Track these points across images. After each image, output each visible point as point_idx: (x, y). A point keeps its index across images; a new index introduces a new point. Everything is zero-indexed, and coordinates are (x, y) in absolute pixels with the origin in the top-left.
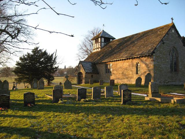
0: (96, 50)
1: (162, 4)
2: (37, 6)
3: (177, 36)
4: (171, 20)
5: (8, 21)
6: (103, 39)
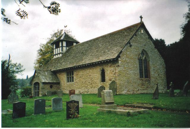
0: (59, 55)
2: (24, 6)
3: (147, 36)
4: (140, 18)
6: (65, 44)
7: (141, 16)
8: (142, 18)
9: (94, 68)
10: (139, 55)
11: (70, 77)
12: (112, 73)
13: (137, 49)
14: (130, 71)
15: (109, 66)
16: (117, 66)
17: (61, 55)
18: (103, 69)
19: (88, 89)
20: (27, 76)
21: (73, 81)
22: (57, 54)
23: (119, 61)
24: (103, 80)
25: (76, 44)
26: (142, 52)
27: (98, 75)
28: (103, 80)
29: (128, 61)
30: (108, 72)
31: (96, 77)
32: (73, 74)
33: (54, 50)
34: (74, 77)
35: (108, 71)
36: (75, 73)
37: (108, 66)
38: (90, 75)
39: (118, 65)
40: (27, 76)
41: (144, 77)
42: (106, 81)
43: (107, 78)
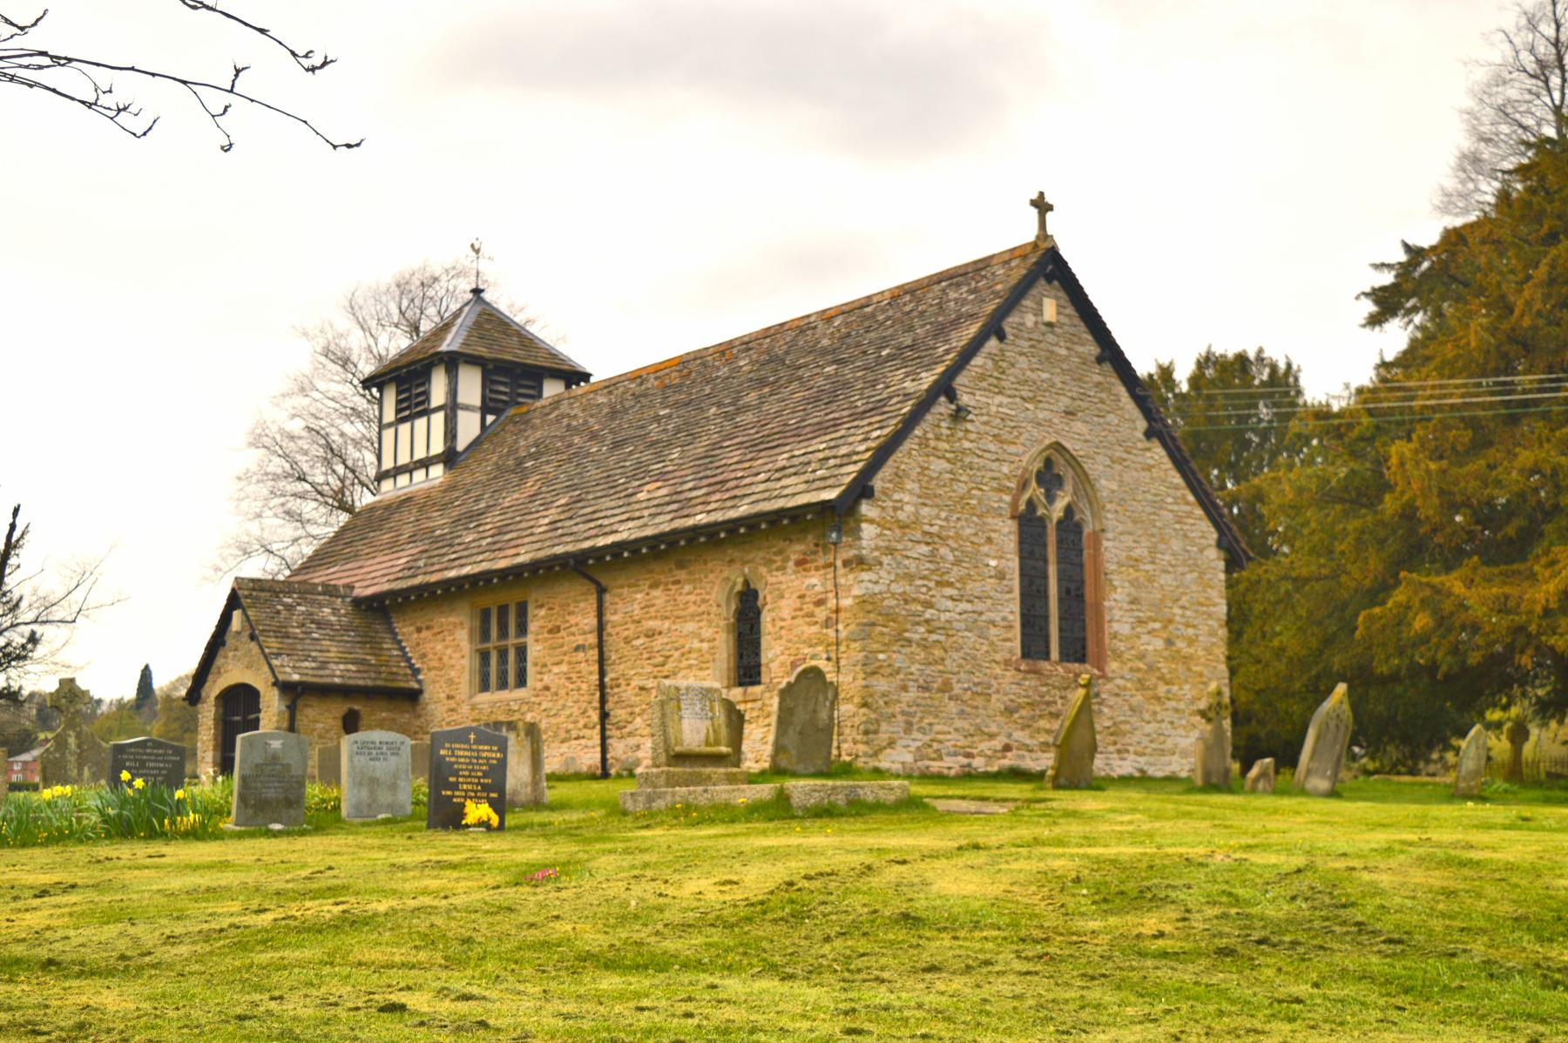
1: (335, 147)
3: (1092, 349)
4: (1034, 212)
5: (604, 760)
6: (471, 386)
7: (1042, 194)
8: (1050, 208)
9: (682, 575)
10: (1024, 485)
11: (503, 654)
12: (811, 615)
13: (1006, 436)
14: (950, 604)
15: (791, 564)
16: (846, 563)
17: (437, 471)
18: (746, 583)
19: (632, 741)
20: (146, 675)
21: (521, 681)
22: (409, 469)
23: (864, 525)
24: (747, 670)
25: (568, 387)
26: (1048, 463)
27: (707, 633)
28: (747, 670)
29: (935, 529)
30: (787, 607)
31: (696, 644)
32: (522, 629)
33: (388, 435)
34: (534, 651)
35: (782, 597)
36: (538, 620)
37: (787, 559)
38: (651, 634)
39: (852, 553)
40: (146, 675)
41: (1055, 654)
42: (765, 678)
43: (776, 657)
